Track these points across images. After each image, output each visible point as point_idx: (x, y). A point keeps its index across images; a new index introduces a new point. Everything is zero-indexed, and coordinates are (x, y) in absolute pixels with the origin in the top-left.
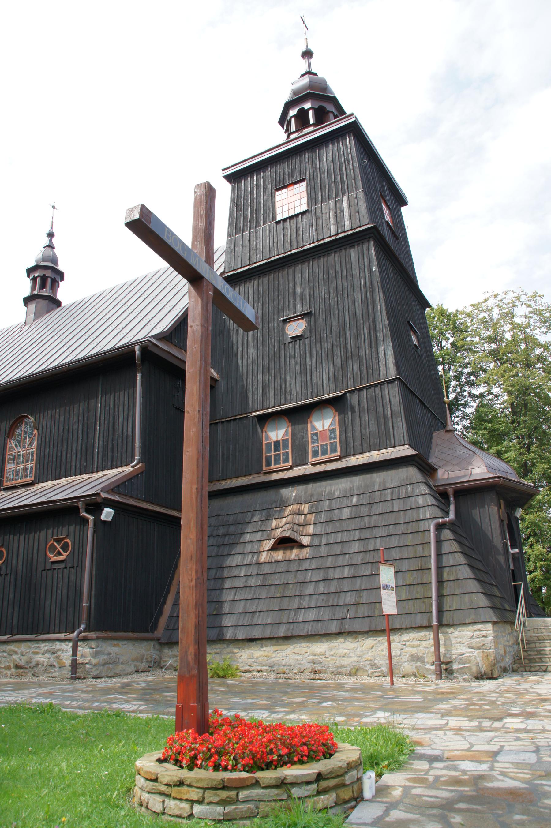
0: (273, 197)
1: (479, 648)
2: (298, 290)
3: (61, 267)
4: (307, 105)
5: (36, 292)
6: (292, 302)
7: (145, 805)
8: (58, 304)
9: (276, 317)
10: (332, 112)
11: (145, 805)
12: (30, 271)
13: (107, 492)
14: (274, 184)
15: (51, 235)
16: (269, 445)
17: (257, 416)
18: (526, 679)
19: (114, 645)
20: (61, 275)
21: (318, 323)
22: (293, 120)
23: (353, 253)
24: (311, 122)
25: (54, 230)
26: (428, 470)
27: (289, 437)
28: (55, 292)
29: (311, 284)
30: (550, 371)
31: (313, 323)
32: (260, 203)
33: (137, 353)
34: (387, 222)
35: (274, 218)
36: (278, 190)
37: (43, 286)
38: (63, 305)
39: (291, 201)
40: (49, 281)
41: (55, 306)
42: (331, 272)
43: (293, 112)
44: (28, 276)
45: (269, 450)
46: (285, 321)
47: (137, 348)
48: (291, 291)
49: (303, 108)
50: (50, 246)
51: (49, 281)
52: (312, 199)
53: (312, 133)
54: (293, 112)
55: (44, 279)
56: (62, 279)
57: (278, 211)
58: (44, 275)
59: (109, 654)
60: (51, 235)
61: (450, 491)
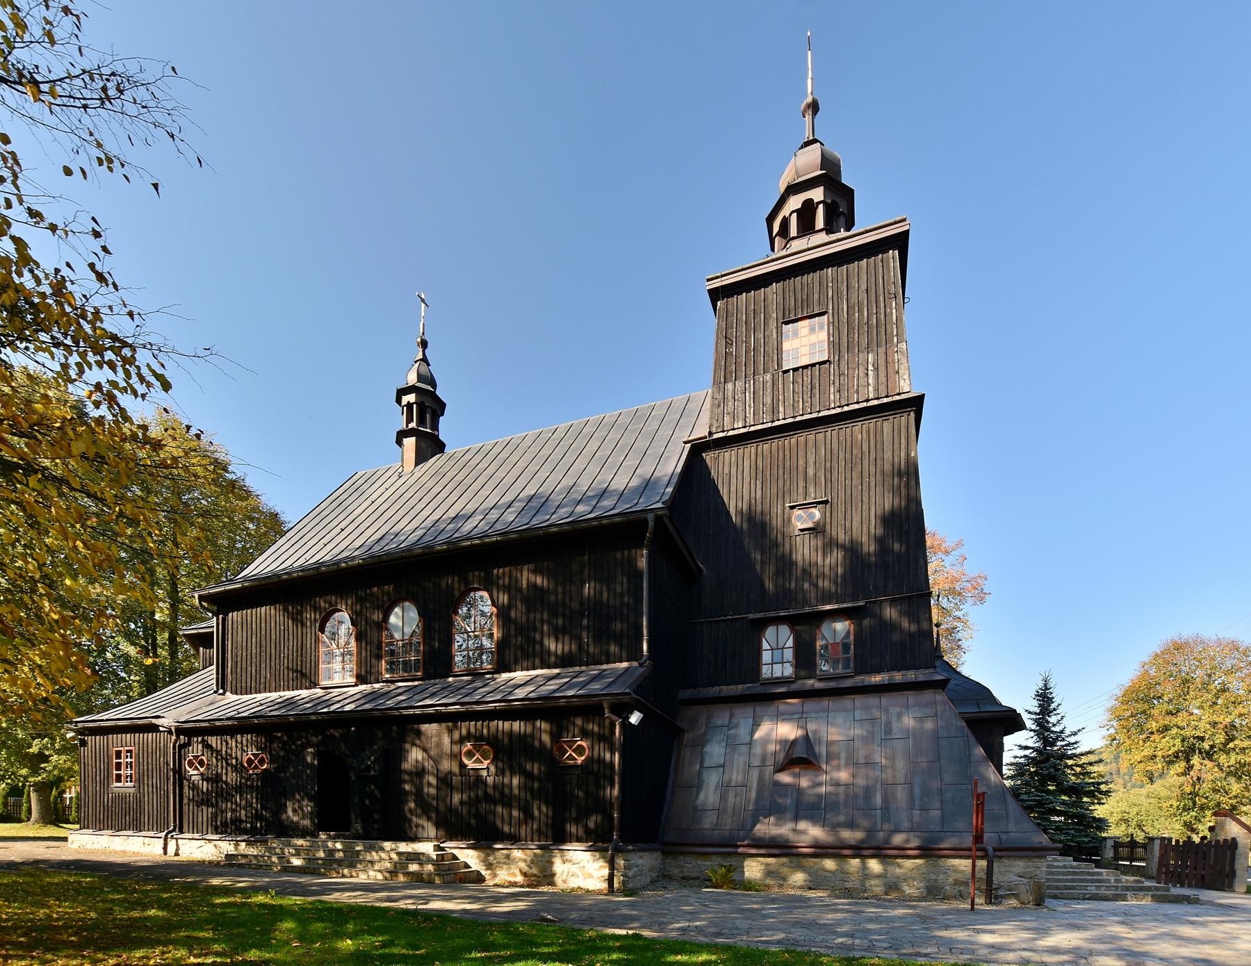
0: (780, 334)
2: (811, 472)
4: (817, 194)
5: (413, 425)
6: (801, 484)
7: (1141, 706)
9: (780, 501)
11: (1141, 706)
14: (780, 315)
15: (424, 344)
17: (752, 620)
20: (442, 406)
21: (835, 515)
22: (795, 215)
23: (887, 426)
25: (426, 337)
28: (435, 426)
29: (828, 465)
30: (6, 958)
31: (828, 514)
32: (759, 339)
33: (651, 524)
35: (779, 365)
36: (787, 323)
39: (805, 343)
42: (855, 451)
43: (795, 202)
46: (792, 508)
47: (651, 517)
48: (801, 469)
49: (811, 200)
50: (424, 360)
52: (834, 345)
53: (819, 243)
54: (795, 202)
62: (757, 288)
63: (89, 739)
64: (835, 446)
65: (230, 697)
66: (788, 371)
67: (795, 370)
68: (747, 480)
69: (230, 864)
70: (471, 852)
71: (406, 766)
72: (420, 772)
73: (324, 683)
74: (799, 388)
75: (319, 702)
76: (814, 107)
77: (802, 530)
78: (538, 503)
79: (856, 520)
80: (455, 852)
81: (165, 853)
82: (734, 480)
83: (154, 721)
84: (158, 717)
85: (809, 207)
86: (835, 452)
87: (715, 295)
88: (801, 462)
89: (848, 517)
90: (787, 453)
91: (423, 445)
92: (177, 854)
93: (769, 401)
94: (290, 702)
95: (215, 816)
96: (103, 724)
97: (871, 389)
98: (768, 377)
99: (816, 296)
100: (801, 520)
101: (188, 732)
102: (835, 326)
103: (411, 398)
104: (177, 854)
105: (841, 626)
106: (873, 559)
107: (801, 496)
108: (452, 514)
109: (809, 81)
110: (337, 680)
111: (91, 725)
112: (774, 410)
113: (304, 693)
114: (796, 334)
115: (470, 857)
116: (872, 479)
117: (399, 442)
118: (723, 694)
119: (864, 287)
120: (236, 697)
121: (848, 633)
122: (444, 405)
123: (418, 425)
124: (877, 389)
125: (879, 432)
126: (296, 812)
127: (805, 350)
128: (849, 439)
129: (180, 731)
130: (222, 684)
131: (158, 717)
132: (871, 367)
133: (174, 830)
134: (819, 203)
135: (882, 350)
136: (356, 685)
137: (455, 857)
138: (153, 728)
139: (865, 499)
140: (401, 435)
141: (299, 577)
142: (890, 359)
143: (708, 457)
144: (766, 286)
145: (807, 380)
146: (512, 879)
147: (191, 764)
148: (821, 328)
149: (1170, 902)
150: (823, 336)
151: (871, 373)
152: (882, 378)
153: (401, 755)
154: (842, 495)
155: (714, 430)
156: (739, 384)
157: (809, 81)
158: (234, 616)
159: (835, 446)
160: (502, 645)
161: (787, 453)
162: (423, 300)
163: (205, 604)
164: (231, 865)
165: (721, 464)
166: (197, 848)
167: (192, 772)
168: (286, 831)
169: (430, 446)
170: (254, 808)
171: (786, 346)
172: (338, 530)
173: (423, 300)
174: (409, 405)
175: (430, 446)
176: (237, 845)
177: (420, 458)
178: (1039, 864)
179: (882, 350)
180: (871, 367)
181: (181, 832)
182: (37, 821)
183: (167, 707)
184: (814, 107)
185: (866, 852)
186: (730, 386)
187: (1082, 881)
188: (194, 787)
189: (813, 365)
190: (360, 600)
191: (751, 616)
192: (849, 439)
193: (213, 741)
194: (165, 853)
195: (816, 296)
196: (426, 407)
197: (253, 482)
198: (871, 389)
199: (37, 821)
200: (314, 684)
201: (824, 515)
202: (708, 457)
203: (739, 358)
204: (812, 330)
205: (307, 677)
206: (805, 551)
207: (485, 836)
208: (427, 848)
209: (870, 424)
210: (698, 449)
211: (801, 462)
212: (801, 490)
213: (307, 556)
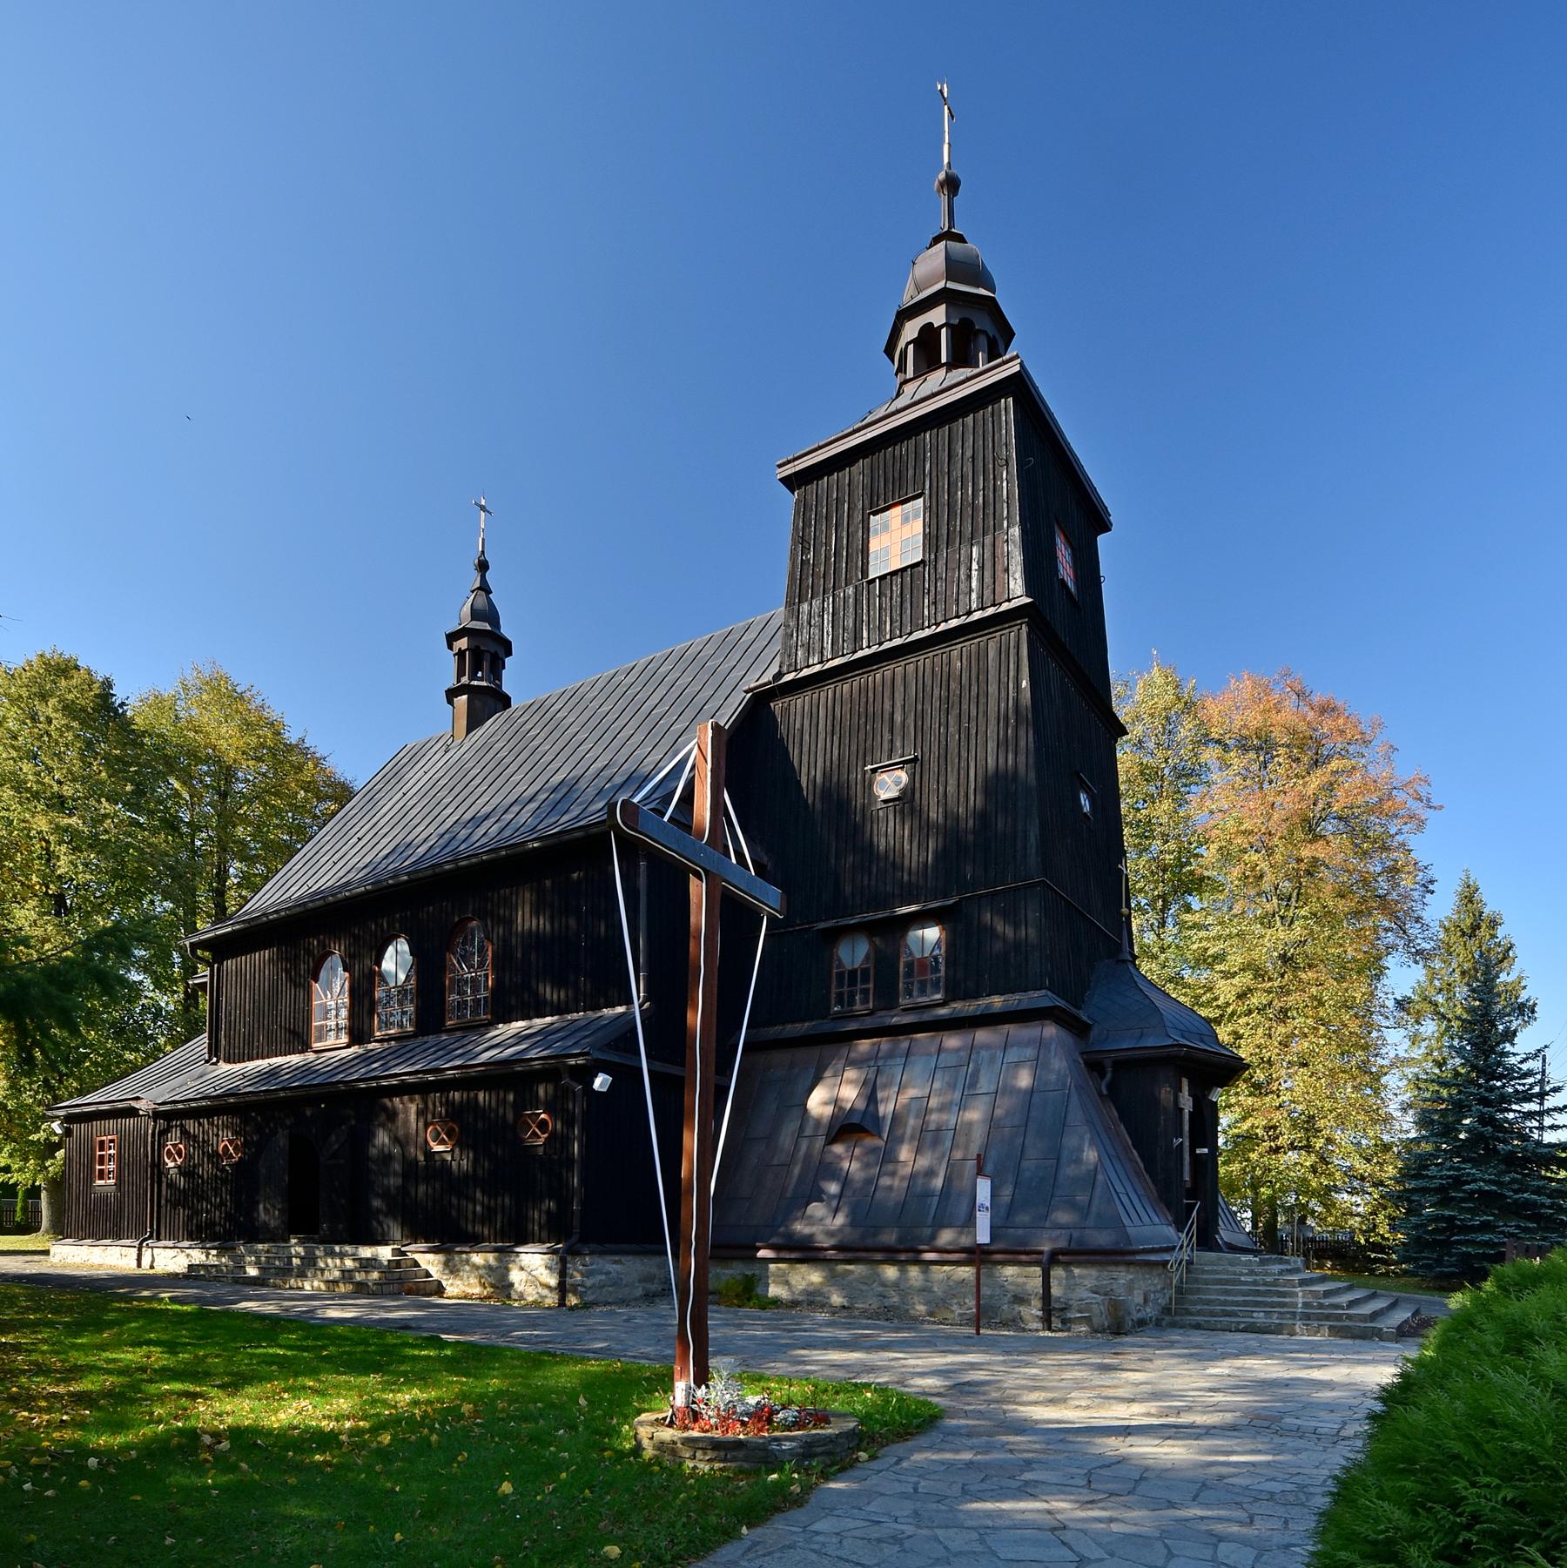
1: (1106, 1294)
2: (898, 718)
3: (505, 631)
4: (937, 316)
5: (465, 680)
6: (887, 737)
8: (505, 702)
10: (985, 333)
12: (452, 638)
13: (600, 1050)
14: (867, 502)
15: (483, 566)
16: (840, 975)
18: (901, 1383)
19: (615, 1262)
20: (507, 647)
21: (926, 777)
22: (911, 347)
24: (944, 360)
26: (1077, 1028)
27: (870, 965)
34: (1063, 582)
35: (865, 572)
36: (875, 513)
37: (476, 666)
38: (514, 705)
40: (487, 657)
41: (500, 706)
42: (953, 685)
44: (450, 647)
45: (840, 984)
46: (874, 771)
48: (886, 716)
49: (931, 324)
50: (484, 588)
51: (487, 657)
52: (931, 540)
54: (911, 330)
55: (476, 653)
56: (509, 653)
57: (871, 569)
58: (478, 647)
59: (609, 1273)
60: (483, 566)
61: (1108, 1063)
62: (840, 469)
63: (74, 1127)
64: (928, 682)
65: (224, 1067)
66: (873, 580)
67: (882, 578)
68: (821, 737)
69: (193, 1275)
70: (431, 1256)
71: (373, 1152)
72: (387, 1158)
73: (316, 1045)
74: (886, 602)
75: (306, 1070)
76: (952, 185)
77: (885, 801)
78: (566, 792)
79: (952, 781)
80: (417, 1256)
81: (139, 1265)
82: (806, 737)
83: (133, 1104)
84: (138, 1098)
85: (929, 332)
86: (928, 689)
87: (791, 482)
88: (887, 706)
89: (942, 779)
90: (871, 694)
91: (478, 703)
92: (152, 1267)
93: (850, 623)
94: (274, 1073)
95: (190, 1218)
96: (86, 1109)
97: (974, 596)
98: (851, 590)
99: (911, 472)
100: (889, 785)
101: (169, 1116)
102: (932, 513)
103: (463, 643)
104: (152, 1267)
105: (932, 934)
106: (971, 837)
107: (885, 755)
108: (468, 816)
109: (946, 147)
110: (331, 1041)
111: (77, 1110)
112: (857, 638)
113: (295, 1059)
114: (886, 527)
115: (430, 1263)
116: (973, 724)
117: (450, 702)
118: (1023, 1006)
119: (969, 453)
120: (229, 1066)
121: (938, 942)
122: (510, 643)
123: (471, 679)
124: (981, 597)
125: (982, 654)
126: (268, 1214)
127: (896, 550)
128: (946, 669)
129: (156, 1115)
130: (214, 1049)
131: (138, 1098)
132: (975, 566)
133: (150, 1237)
134: (941, 327)
135: (988, 539)
136: (348, 1047)
137: (416, 1264)
138: (132, 1112)
139: (964, 754)
140: (451, 694)
141: (288, 916)
142: (998, 552)
143: (777, 706)
144: (851, 464)
145: (896, 589)
146: (470, 1291)
147: (169, 1154)
148: (916, 517)
149: (1354, 1337)
150: (918, 526)
151: (974, 573)
152: (988, 579)
153: (370, 1136)
154: (935, 748)
155: (785, 669)
156: (816, 603)
157: (946, 147)
158: (230, 964)
159: (928, 682)
160: (497, 990)
161: (871, 694)
162: (483, 508)
163: (199, 952)
164: (197, 1278)
165: (793, 712)
166: (170, 1259)
167: (441, 1148)
168: (253, 1234)
169: (486, 702)
170: (216, 1208)
171: (874, 545)
172: (355, 840)
173: (483, 508)
174: (461, 654)
175: (486, 702)
176: (207, 1255)
177: (474, 723)
178: (1115, 1274)
179: (988, 539)
180: (975, 566)
181: (159, 1239)
182: (47, 1232)
183: (148, 1086)
184: (952, 185)
185: (903, 1257)
186: (805, 606)
187: (1245, 1303)
188: (171, 1185)
189: (903, 570)
190: (356, 938)
191: (822, 925)
192: (946, 669)
193: (191, 1125)
194: (139, 1265)
195: (911, 472)
196: (483, 650)
197: (318, 743)
198: (974, 596)
199: (47, 1232)
200: (305, 1047)
201: (912, 777)
202: (777, 706)
203: (824, 560)
204: (905, 519)
205: (299, 1039)
206: (890, 834)
207: (451, 1237)
208: (385, 1253)
209: (969, 645)
210: (760, 701)
211: (887, 706)
212: (886, 746)
213: (310, 883)
